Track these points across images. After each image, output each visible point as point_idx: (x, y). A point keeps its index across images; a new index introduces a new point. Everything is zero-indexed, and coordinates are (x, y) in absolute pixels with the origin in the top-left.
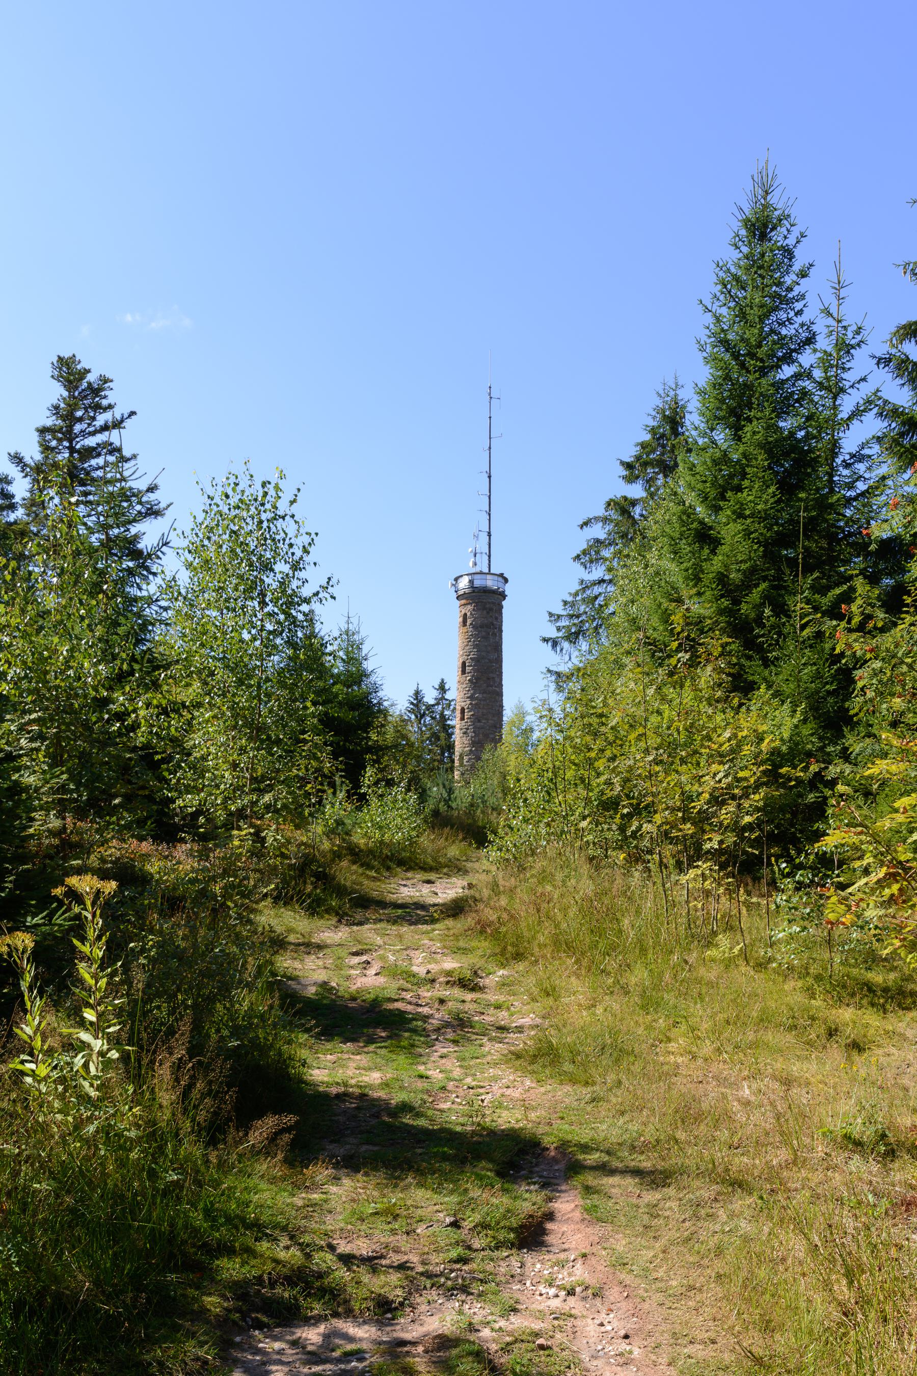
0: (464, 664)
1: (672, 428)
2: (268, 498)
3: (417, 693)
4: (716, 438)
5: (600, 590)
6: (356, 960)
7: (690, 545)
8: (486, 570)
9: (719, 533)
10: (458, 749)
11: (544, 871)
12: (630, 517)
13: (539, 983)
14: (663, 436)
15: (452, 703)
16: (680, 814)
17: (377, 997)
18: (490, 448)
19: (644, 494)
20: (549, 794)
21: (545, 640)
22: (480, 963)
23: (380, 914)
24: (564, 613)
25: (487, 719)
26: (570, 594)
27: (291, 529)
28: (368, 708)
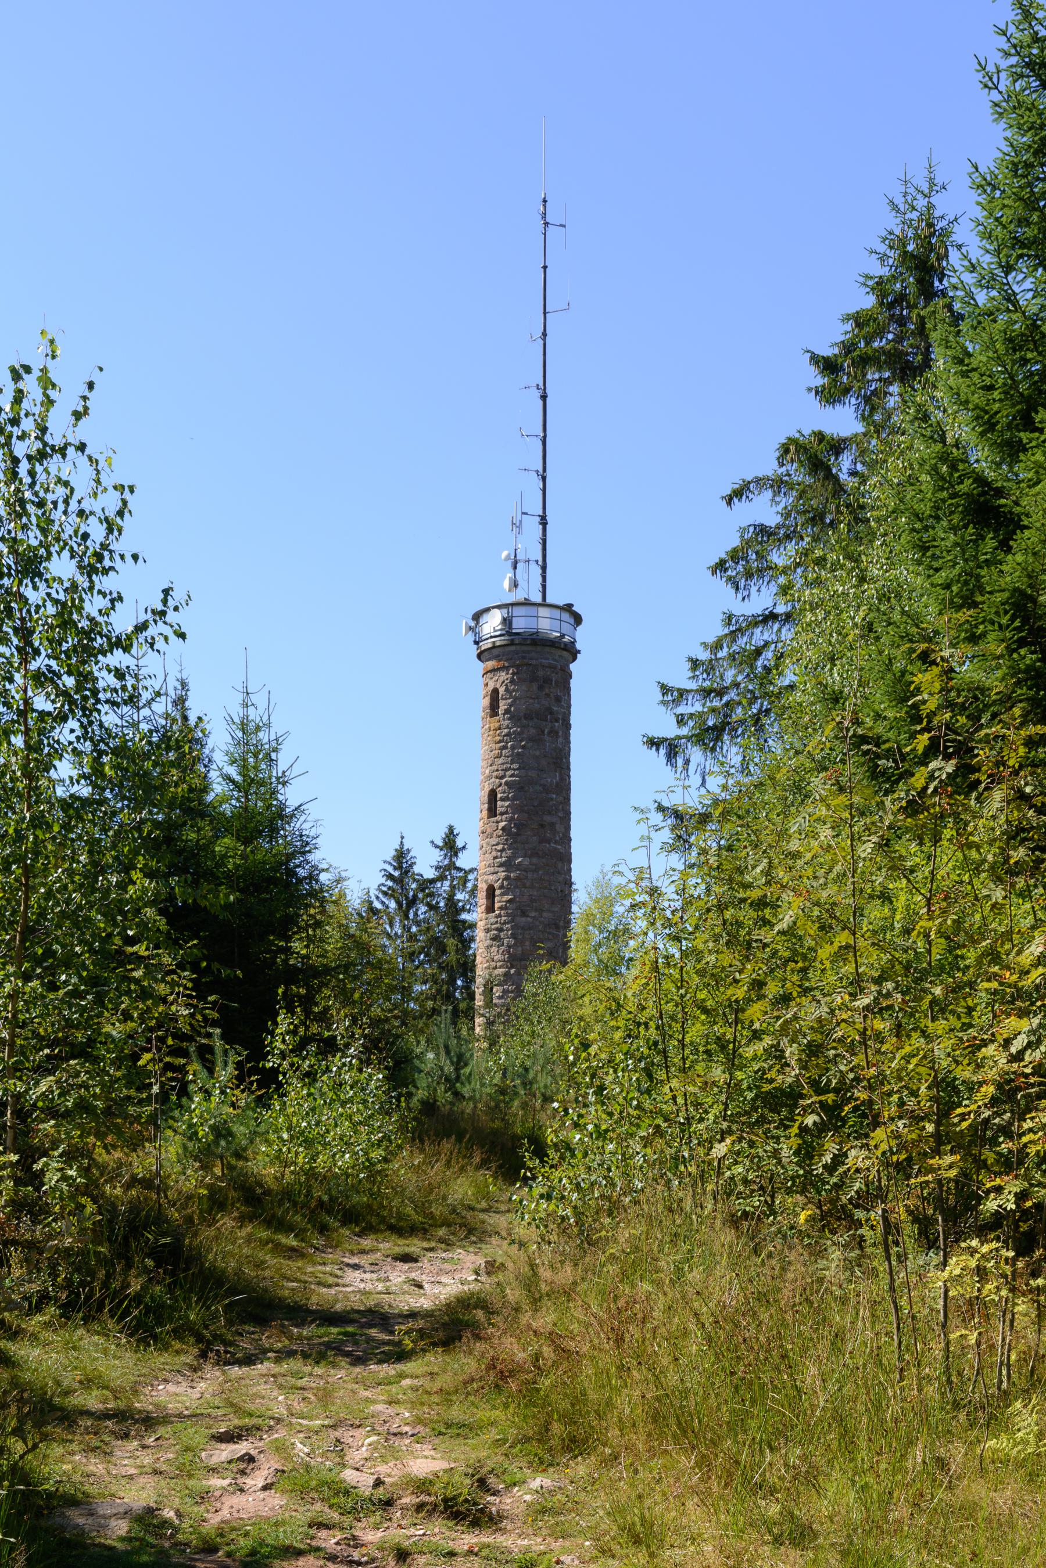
0: (492, 795)
1: (920, 281)
2: (26, 404)
3: (401, 857)
4: (1016, 288)
5: (766, 636)
6: (226, 1452)
7: (954, 529)
8: (537, 598)
9: (1017, 503)
10: (481, 971)
11: (636, 1249)
12: (830, 477)
13: (616, 1511)
14: (901, 298)
15: (471, 877)
16: (930, 1128)
17: (262, 1543)
18: (545, 334)
19: (859, 428)
20: (650, 1076)
21: (653, 743)
22: (495, 1460)
23: (290, 1338)
24: (693, 685)
25: (540, 911)
26: (705, 645)
27: (81, 478)
28: (288, 885)
